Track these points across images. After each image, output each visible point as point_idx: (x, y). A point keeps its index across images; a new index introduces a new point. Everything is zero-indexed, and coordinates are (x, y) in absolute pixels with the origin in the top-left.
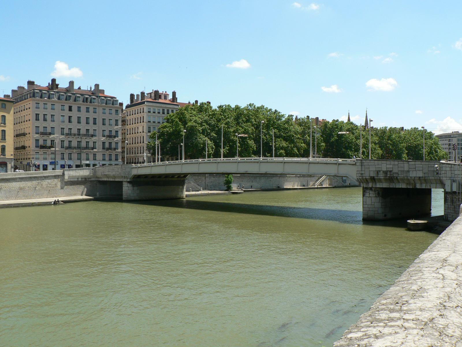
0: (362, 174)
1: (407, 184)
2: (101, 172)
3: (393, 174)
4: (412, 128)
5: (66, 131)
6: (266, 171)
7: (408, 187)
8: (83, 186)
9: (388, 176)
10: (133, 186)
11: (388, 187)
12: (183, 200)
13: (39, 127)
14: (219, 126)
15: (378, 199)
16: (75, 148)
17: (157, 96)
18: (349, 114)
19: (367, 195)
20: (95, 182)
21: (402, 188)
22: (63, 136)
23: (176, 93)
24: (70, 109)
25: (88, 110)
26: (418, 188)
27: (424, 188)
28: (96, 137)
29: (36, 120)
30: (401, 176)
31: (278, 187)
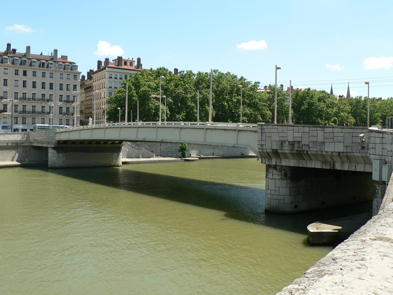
0: (262, 145)
1: (323, 162)
2: (33, 137)
3: (302, 147)
4: (388, 98)
5: (20, 95)
6: (162, 139)
7: (324, 168)
8: (14, 152)
9: (296, 149)
10: (58, 152)
11: (297, 165)
12: (118, 169)
13: (7, 92)
14: (176, 92)
15: (284, 183)
16: (29, 113)
17: (120, 62)
18: (332, 85)
19: (270, 176)
20: (29, 147)
21: (315, 168)
22: (16, 101)
23: (141, 59)
24: (25, 73)
25: (44, 75)
26: (338, 169)
27: (347, 169)
28: (52, 102)
29: (4, 85)
30: (313, 150)
31: (242, 154)
